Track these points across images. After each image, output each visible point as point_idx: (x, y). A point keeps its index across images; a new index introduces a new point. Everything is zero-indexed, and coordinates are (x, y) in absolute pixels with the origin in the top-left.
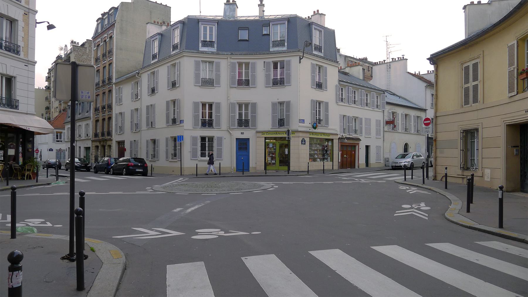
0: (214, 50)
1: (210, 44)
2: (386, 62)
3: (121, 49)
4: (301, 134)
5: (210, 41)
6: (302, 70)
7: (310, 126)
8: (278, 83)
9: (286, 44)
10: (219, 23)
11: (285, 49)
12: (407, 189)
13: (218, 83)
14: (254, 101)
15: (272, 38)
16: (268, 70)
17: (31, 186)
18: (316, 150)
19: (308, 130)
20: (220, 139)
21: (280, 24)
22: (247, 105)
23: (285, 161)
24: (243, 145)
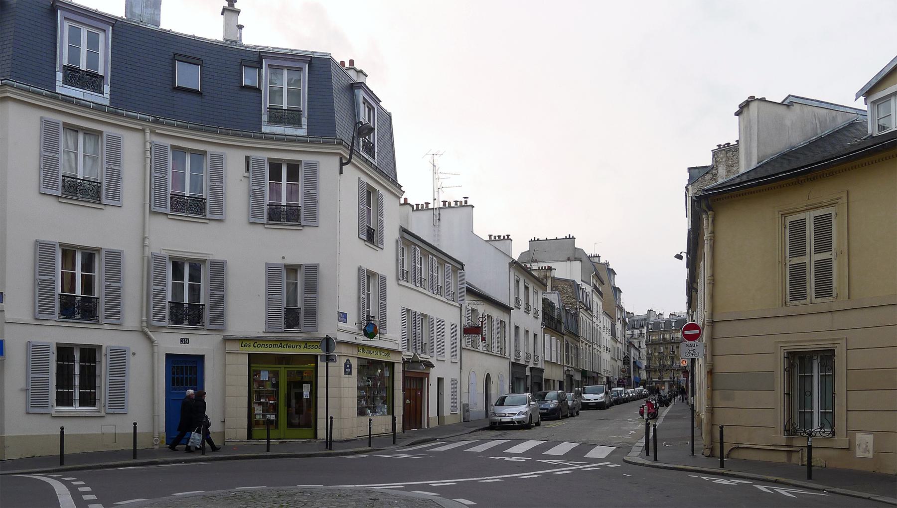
2: (430, 206)
5: (88, 73)
8: (284, 216)
13: (115, 194)
14: (218, 257)
16: (257, 181)
17: (180, 462)
20: (120, 356)
23: (303, 413)
24: (184, 371)
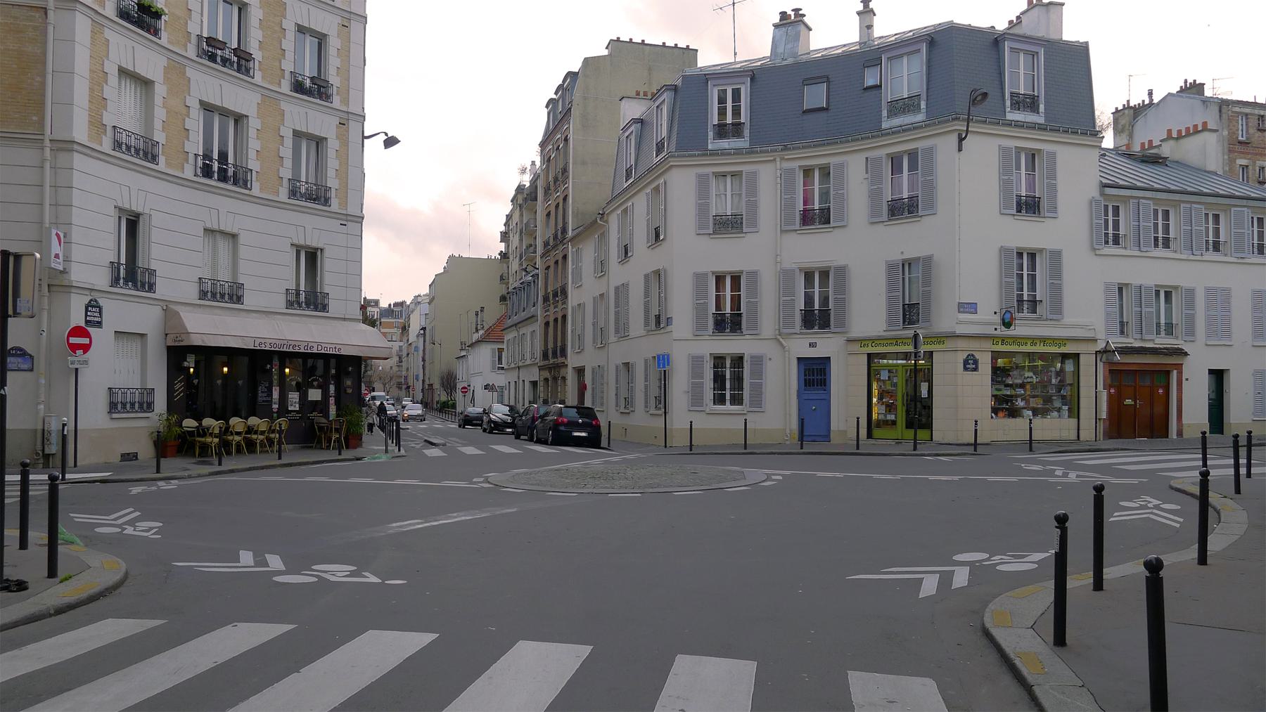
0: (742, 143)
1: (1029, 103)
3: (584, 163)
4: (961, 344)
6: (971, 171)
7: (997, 319)
8: (903, 209)
10: (755, 75)
11: (920, 117)
12: (132, 523)
13: (754, 223)
14: (841, 263)
15: (888, 95)
17: (323, 462)
18: (1022, 386)
19: (990, 330)
20: (758, 361)
21: (909, 54)
22: (825, 274)
23: (919, 414)
24: (815, 374)
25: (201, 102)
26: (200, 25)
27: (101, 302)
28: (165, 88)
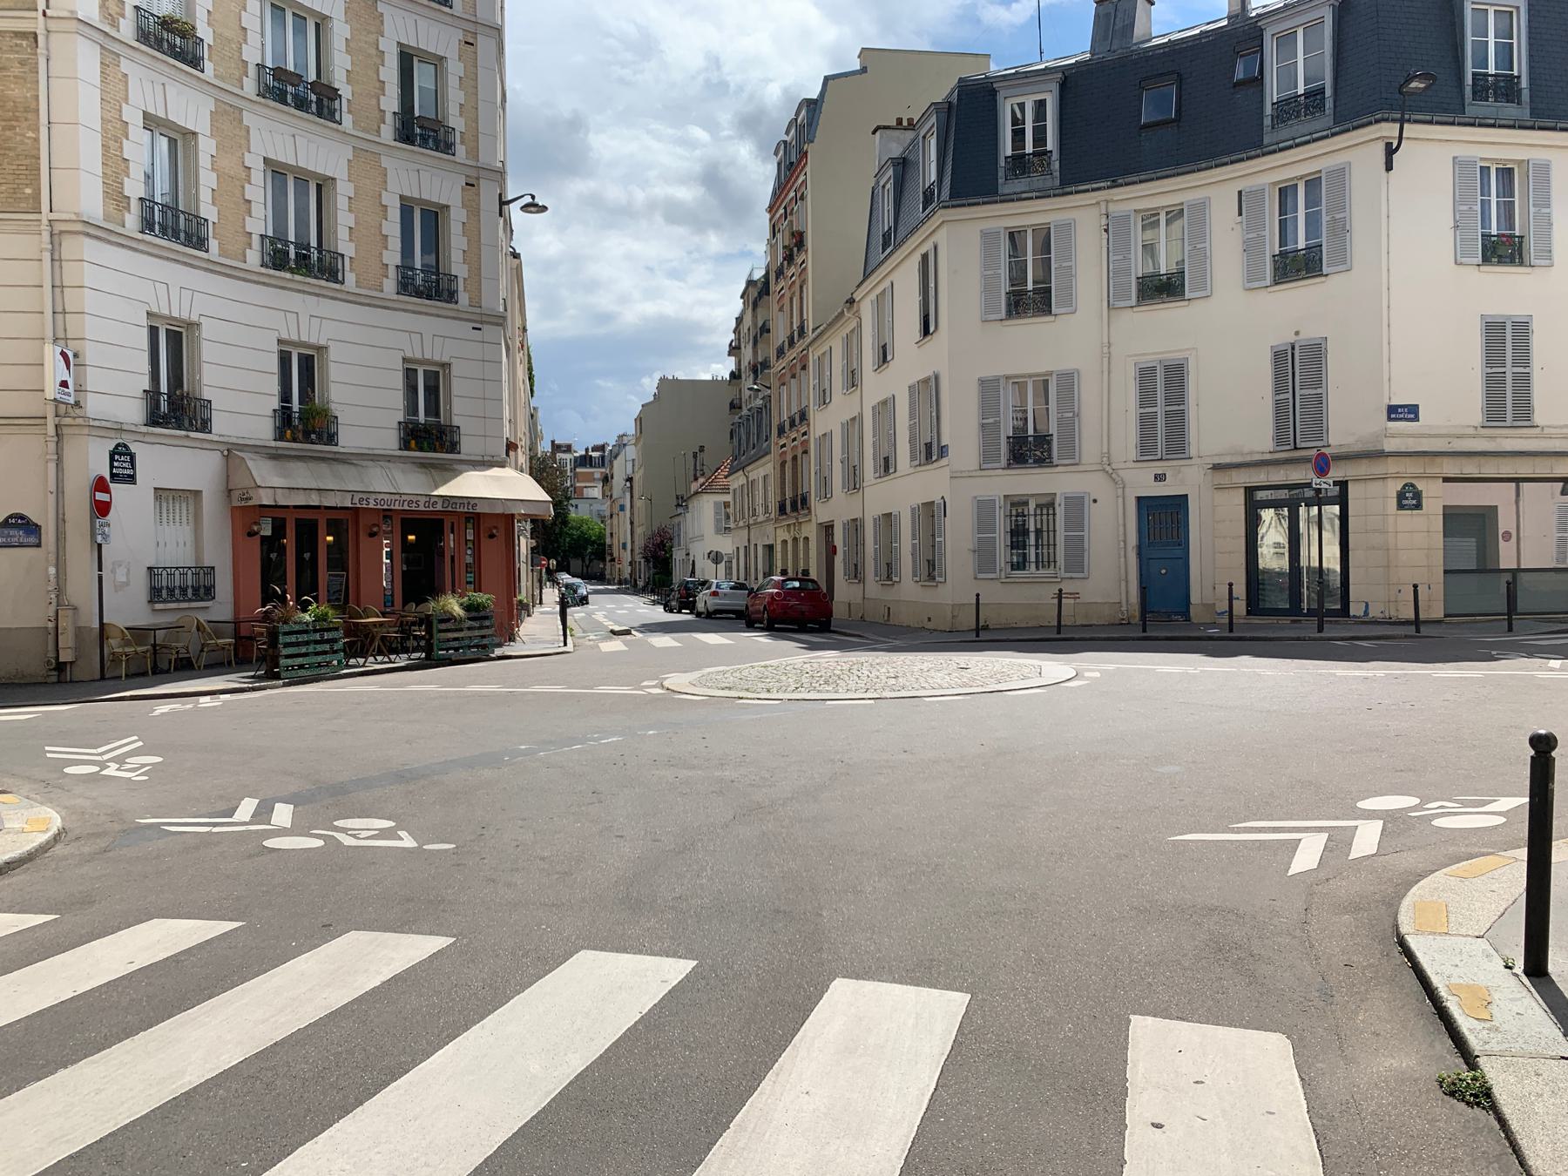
4: (1392, 466)
8: (1297, 265)
9: (1329, 104)
20: (1077, 504)
25: (146, 116)
26: (258, 48)
27: (133, 448)
28: (213, 142)
